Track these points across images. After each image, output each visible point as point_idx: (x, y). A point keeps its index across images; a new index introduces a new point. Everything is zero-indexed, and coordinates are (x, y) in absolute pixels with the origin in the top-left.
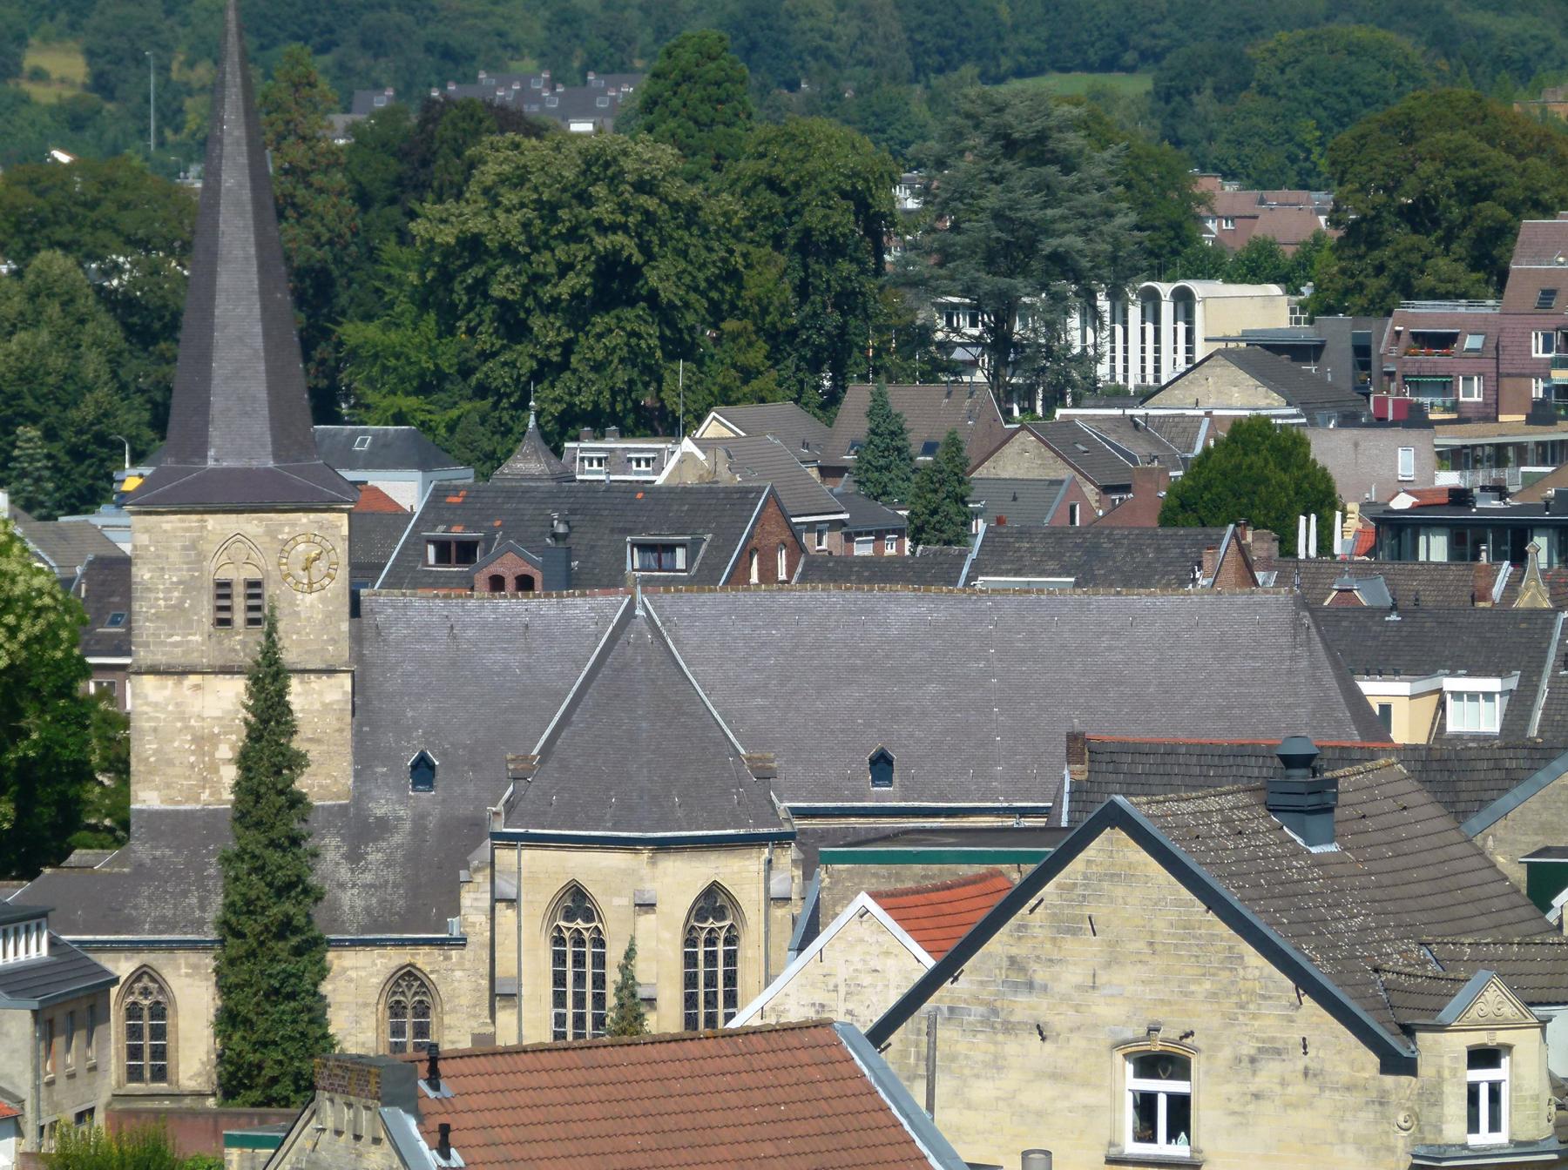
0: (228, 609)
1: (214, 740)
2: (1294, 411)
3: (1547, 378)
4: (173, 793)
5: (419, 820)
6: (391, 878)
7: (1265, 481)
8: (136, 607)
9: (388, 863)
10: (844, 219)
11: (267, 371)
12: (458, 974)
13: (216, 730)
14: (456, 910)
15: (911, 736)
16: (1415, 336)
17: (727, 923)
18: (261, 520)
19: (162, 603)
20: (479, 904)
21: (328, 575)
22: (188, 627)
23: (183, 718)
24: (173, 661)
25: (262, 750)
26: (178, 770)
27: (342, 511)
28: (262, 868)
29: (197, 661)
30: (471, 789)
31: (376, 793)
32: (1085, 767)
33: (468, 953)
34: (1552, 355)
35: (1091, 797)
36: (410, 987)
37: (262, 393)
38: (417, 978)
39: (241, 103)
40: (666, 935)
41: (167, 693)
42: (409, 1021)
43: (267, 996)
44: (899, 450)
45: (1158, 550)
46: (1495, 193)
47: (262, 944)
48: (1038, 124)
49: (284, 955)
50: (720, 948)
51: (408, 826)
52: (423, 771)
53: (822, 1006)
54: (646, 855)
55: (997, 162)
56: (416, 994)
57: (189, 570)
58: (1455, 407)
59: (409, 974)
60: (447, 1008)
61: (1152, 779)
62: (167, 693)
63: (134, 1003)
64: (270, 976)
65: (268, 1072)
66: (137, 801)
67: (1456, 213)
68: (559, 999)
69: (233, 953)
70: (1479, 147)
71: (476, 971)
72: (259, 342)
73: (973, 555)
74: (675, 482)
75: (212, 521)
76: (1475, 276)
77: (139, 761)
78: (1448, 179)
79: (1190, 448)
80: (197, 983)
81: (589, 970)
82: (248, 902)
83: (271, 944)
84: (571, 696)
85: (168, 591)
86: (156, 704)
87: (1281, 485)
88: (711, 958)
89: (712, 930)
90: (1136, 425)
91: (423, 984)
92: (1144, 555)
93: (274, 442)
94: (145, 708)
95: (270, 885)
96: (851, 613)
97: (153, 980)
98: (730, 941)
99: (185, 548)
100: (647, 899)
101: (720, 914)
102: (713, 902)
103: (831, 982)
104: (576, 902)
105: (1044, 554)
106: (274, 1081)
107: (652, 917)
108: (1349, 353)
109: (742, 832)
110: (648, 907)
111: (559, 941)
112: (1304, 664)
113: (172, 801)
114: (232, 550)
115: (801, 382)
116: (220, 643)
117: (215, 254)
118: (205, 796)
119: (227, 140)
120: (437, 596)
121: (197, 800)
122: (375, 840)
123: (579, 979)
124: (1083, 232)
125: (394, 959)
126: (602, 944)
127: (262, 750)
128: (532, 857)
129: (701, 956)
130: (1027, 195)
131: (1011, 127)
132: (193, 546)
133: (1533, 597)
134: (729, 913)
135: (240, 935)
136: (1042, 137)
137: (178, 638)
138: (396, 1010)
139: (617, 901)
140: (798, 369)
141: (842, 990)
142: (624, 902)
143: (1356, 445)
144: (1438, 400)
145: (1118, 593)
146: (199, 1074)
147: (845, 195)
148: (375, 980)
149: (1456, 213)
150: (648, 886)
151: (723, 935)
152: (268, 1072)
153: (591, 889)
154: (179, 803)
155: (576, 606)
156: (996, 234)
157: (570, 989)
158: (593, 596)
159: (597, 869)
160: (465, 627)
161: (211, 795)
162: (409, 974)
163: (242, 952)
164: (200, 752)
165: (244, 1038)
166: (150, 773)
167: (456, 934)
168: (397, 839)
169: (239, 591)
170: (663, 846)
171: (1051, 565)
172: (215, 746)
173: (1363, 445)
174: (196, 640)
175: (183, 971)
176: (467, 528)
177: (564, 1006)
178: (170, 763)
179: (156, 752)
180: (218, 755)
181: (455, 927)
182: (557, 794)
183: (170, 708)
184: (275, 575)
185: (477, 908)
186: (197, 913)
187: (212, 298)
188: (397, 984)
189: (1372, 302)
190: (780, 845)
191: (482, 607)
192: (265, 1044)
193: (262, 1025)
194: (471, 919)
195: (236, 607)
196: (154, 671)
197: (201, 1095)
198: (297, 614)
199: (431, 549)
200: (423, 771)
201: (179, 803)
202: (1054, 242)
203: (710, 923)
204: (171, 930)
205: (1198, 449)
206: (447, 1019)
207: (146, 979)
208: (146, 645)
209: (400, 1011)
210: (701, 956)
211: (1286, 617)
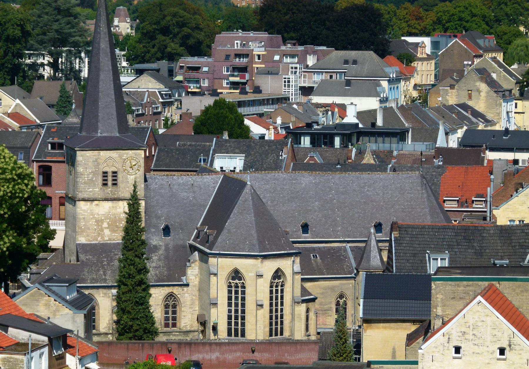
0: (106, 180)
1: (102, 221)
2: (167, 90)
3: (228, 79)
4: (89, 238)
5: (167, 246)
6: (161, 265)
7: (227, 117)
9: (159, 260)
10: (18, 32)
11: (116, 105)
12: (186, 295)
13: (103, 218)
14: (184, 274)
15: (312, 218)
16: (188, 67)
17: (281, 280)
18: (117, 153)
21: (138, 170)
23: (93, 214)
24: (90, 197)
25: (133, 227)
26: (91, 231)
27: (142, 150)
28: (134, 264)
30: (181, 236)
31: (152, 237)
32: (398, 233)
33: (189, 288)
34: (229, 73)
35: (401, 242)
36: (171, 299)
37: (115, 113)
38: (173, 296)
39: (106, 21)
40: (266, 285)
41: (88, 207)
42: (170, 310)
44: (69, 102)
45: (269, 146)
46: (187, 25)
47: (133, 288)
48: (68, 5)
49: (140, 291)
50: (279, 288)
51: (163, 248)
52: (167, 231)
53: (465, 332)
54: (260, 260)
55: (56, 16)
56: (173, 301)
58: (200, 87)
60: (183, 305)
61: (419, 236)
62: (88, 207)
64: (136, 298)
65: (135, 328)
66: (78, 241)
67: (176, 30)
68: (230, 305)
69: (124, 291)
70: (182, 12)
72: (113, 97)
73: (213, 147)
74: (14, 111)
75: (102, 153)
76: (182, 48)
78: (174, 22)
79: (143, 100)
81: (240, 296)
82: (129, 275)
83: (136, 287)
84: (208, 206)
85: (88, 175)
86: (84, 210)
87: (231, 118)
88: (277, 291)
89: (277, 282)
90: (127, 94)
91: (175, 298)
92: (265, 148)
93: (119, 128)
94: (81, 212)
95: (136, 269)
96: (290, 180)
98: (282, 286)
99: (93, 161)
100: (260, 274)
101: (279, 278)
102: (278, 274)
103: (468, 325)
104: (236, 274)
105: (234, 147)
106: (137, 330)
107: (262, 279)
108: (167, 71)
109: (286, 252)
110: (261, 276)
111: (230, 286)
112: (425, 195)
113: (89, 240)
115: (5, 78)
117: (99, 69)
118: (99, 239)
119: (102, 33)
120: (164, 175)
121: (97, 240)
122: (154, 252)
123: (237, 298)
124: (80, 36)
125: (166, 290)
126: (244, 287)
127: (133, 227)
128: (222, 261)
129: (274, 291)
130: (65, 25)
131: (60, 6)
132: (96, 160)
133: (368, 159)
134: (282, 277)
135: (126, 285)
136: (68, 9)
138: (167, 306)
139: (250, 274)
140: (4, 74)
141: (471, 327)
142: (253, 274)
143: (201, 101)
144: (195, 85)
145: (369, 174)
146: (106, 327)
147: (18, 25)
149: (176, 30)
150: (260, 270)
151: (280, 284)
152: (135, 328)
153: (242, 270)
154: (91, 241)
155: (207, 178)
156: (57, 36)
157: (233, 301)
158: (212, 175)
160: (174, 185)
161: (101, 238)
163: (127, 290)
164: (98, 225)
165: (127, 317)
167: (185, 283)
168: (161, 252)
169: (110, 175)
170: (265, 257)
171: (237, 151)
172: (103, 223)
173: (203, 101)
174: (97, 190)
175: (101, 295)
176: (59, 139)
179: (84, 225)
181: (184, 280)
182: (228, 240)
184: (121, 169)
185: (192, 274)
186: (104, 277)
187: (98, 82)
188: (167, 298)
189: (152, 55)
190: (297, 256)
191: (178, 178)
192: (134, 319)
193: (133, 313)
194: (190, 278)
196: (84, 200)
197: (107, 334)
198: (128, 182)
199: (50, 145)
201: (91, 241)
202: (73, 39)
203: (276, 281)
204: (97, 282)
205: (145, 101)
206: (183, 309)
208: (81, 192)
210: (274, 291)
211: (419, 180)
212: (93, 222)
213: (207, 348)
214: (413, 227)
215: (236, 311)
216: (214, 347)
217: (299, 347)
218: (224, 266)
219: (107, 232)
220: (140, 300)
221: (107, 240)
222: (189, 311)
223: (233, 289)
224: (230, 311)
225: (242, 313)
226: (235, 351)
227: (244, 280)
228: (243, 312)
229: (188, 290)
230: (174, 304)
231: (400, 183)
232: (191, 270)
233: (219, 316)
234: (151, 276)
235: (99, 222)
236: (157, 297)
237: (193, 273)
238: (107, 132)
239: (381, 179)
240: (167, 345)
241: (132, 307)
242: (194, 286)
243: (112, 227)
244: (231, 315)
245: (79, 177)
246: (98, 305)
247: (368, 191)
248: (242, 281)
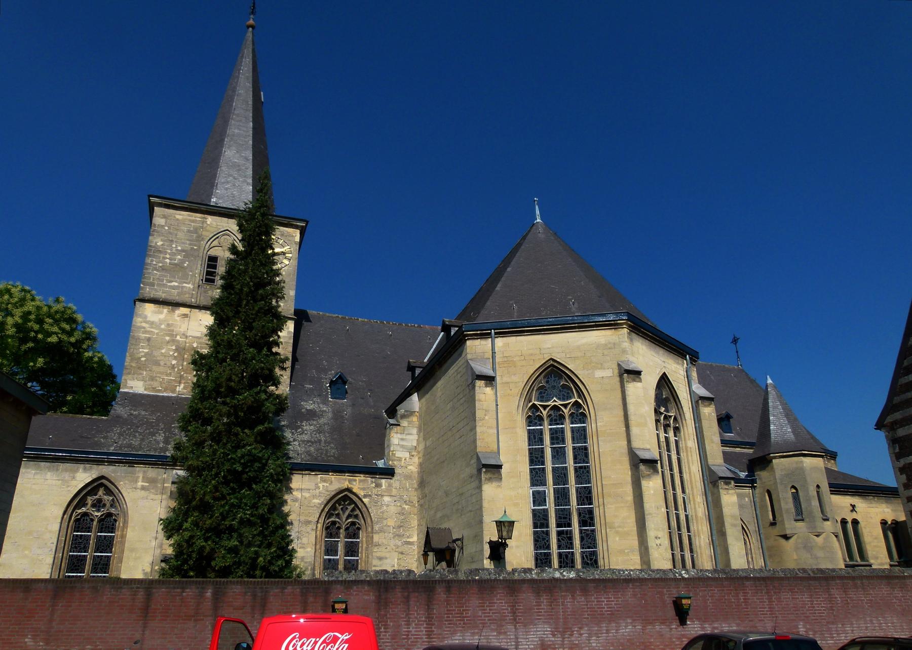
4: (156, 384)
6: (323, 439)
9: (319, 431)
11: (254, 128)
12: (387, 499)
19: (168, 261)
22: (184, 278)
23: (172, 335)
27: (296, 227)
33: (395, 482)
38: (352, 502)
41: (162, 316)
43: (226, 483)
52: (339, 384)
56: (349, 516)
57: (190, 244)
59: (346, 498)
60: (376, 527)
62: (162, 316)
63: (85, 514)
65: (218, 563)
66: (126, 387)
71: (401, 497)
75: (210, 219)
77: (132, 360)
80: (152, 496)
81: (569, 446)
94: (144, 325)
97: (109, 492)
104: (554, 378)
113: (154, 389)
121: (174, 391)
125: (335, 483)
132: (196, 230)
137: (176, 284)
138: (331, 530)
139: (599, 374)
142: (609, 373)
148: (316, 501)
162: (346, 498)
165: (196, 524)
166: (139, 368)
175: (140, 484)
177: (543, 483)
178: (157, 363)
179: (146, 355)
183: (163, 326)
185: (402, 446)
188: (334, 508)
194: (398, 454)
200: (339, 384)
201: (159, 391)
206: (376, 538)
207: (101, 492)
208: (153, 285)
209: (334, 531)
212: (170, 350)
213: (500, 602)
215: (562, 496)
216: (527, 597)
217: (837, 594)
218: (511, 358)
220: (244, 465)
222: (392, 543)
223: (546, 427)
224: (539, 498)
225: (580, 501)
226: (613, 617)
227: (581, 394)
228: (586, 496)
230: (353, 523)
232: (399, 436)
233: (509, 498)
234: (299, 442)
236: (306, 496)
237: (404, 444)
240: (327, 592)
241: (216, 488)
242: (408, 477)
244: (546, 511)
245: (150, 256)
246: (125, 515)
248: (573, 400)
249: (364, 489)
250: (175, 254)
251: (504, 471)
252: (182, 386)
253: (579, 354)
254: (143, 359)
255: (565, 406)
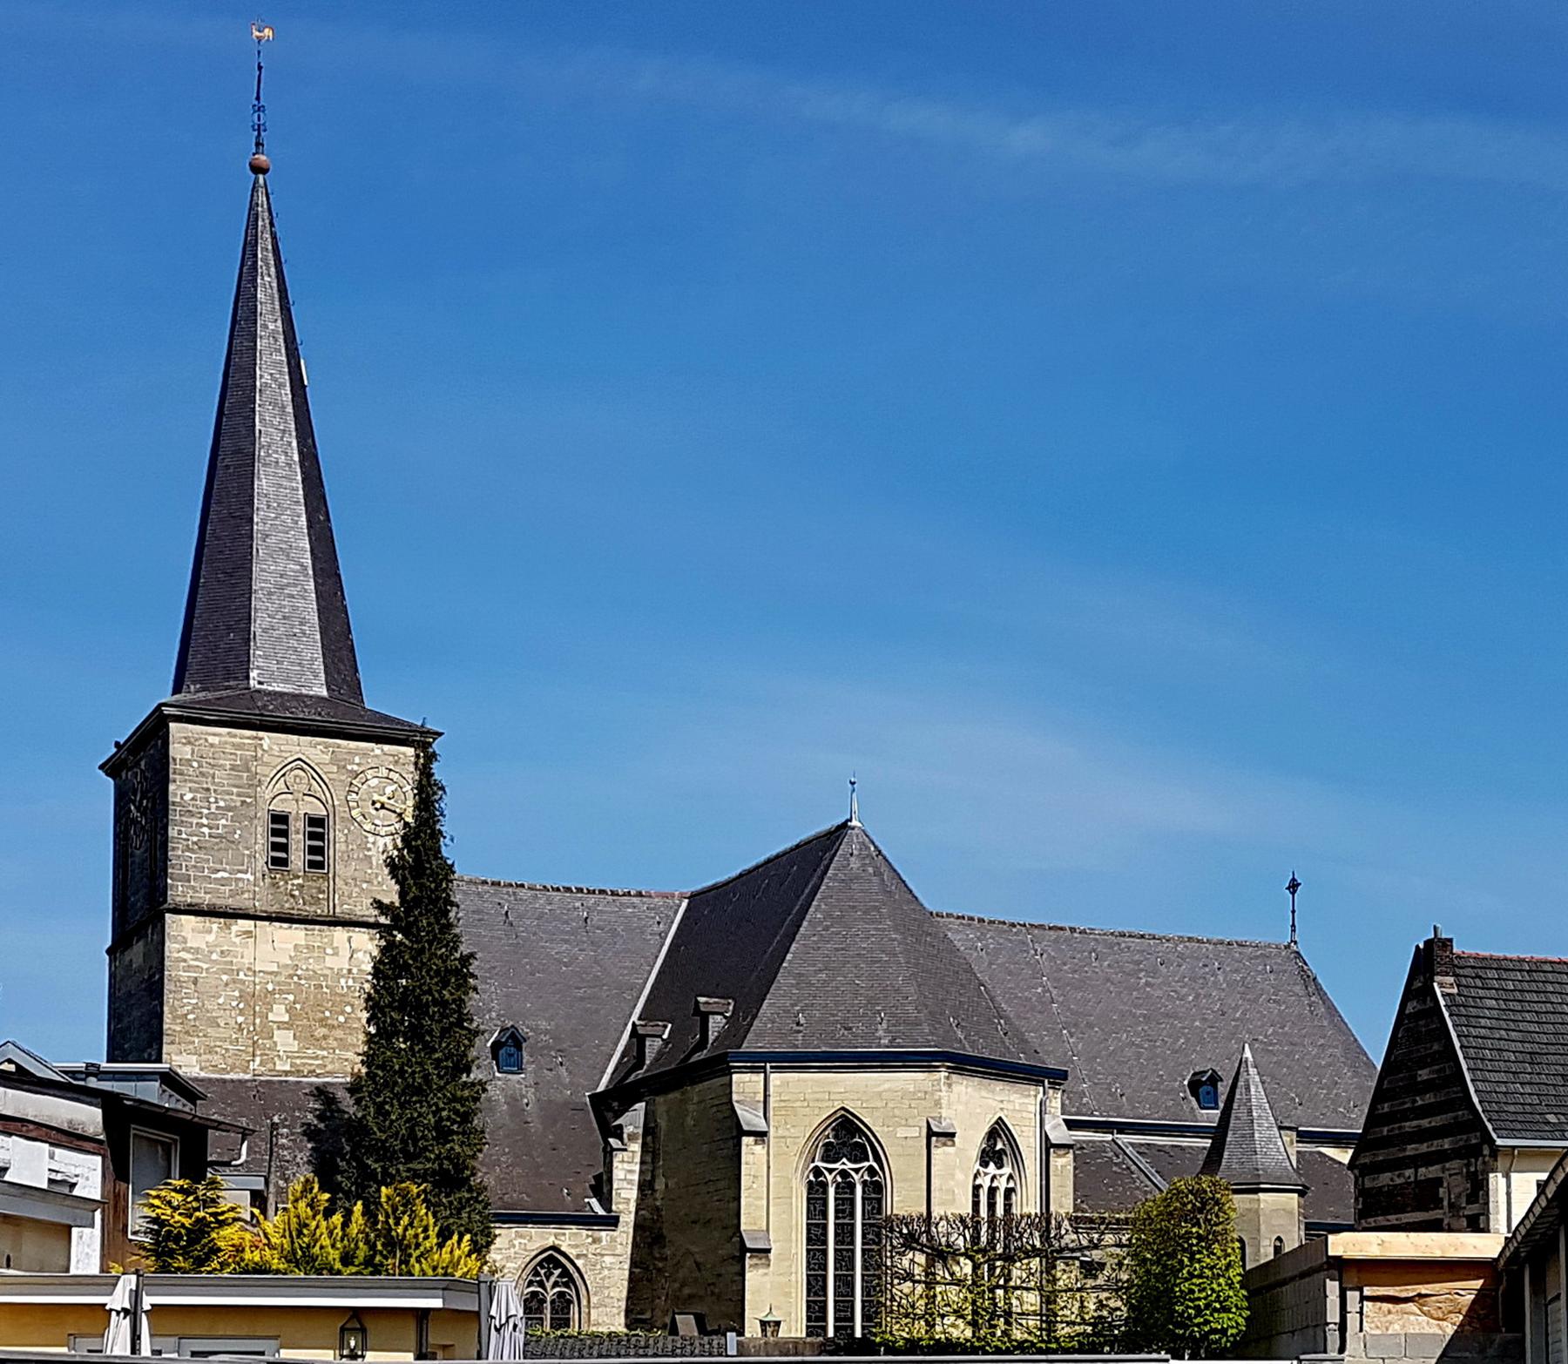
8: (172, 832)
20: (629, 1177)
24: (219, 902)
29: (249, 904)
38: (558, 1264)
41: (211, 938)
56: (556, 1284)
62: (211, 938)
91: (565, 1273)
94: (183, 955)
104: (847, 1136)
114: (290, 778)
116: (275, 885)
125: (540, 1238)
137: (226, 875)
139: (901, 1132)
159: (867, 1093)
162: (550, 1259)
174: (248, 881)
180: (271, 1017)
182: (802, 1011)
183: (214, 957)
195: (293, 847)
196: (194, 911)
214: (1500, 965)
219: (285, 1041)
221: (286, 1073)
227: (877, 1159)
229: (613, 1240)
231: (1237, 971)
235: (254, 1001)
238: (286, 681)
239: (1181, 956)
243: (310, 1020)
247: (1147, 984)
249: (577, 1246)
250: (215, 817)
251: (771, 1256)
252: (258, 1059)
253: (879, 1104)
254: (191, 1017)
255: (857, 1170)
